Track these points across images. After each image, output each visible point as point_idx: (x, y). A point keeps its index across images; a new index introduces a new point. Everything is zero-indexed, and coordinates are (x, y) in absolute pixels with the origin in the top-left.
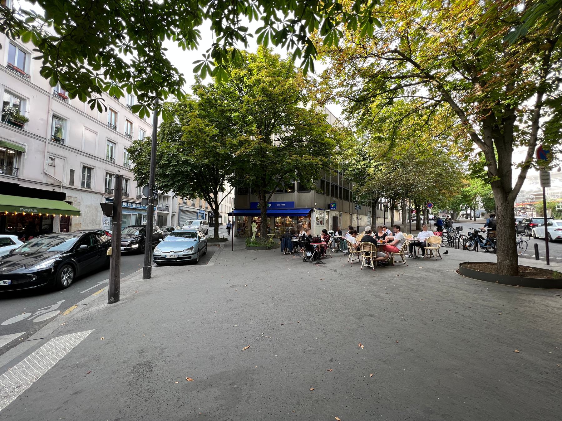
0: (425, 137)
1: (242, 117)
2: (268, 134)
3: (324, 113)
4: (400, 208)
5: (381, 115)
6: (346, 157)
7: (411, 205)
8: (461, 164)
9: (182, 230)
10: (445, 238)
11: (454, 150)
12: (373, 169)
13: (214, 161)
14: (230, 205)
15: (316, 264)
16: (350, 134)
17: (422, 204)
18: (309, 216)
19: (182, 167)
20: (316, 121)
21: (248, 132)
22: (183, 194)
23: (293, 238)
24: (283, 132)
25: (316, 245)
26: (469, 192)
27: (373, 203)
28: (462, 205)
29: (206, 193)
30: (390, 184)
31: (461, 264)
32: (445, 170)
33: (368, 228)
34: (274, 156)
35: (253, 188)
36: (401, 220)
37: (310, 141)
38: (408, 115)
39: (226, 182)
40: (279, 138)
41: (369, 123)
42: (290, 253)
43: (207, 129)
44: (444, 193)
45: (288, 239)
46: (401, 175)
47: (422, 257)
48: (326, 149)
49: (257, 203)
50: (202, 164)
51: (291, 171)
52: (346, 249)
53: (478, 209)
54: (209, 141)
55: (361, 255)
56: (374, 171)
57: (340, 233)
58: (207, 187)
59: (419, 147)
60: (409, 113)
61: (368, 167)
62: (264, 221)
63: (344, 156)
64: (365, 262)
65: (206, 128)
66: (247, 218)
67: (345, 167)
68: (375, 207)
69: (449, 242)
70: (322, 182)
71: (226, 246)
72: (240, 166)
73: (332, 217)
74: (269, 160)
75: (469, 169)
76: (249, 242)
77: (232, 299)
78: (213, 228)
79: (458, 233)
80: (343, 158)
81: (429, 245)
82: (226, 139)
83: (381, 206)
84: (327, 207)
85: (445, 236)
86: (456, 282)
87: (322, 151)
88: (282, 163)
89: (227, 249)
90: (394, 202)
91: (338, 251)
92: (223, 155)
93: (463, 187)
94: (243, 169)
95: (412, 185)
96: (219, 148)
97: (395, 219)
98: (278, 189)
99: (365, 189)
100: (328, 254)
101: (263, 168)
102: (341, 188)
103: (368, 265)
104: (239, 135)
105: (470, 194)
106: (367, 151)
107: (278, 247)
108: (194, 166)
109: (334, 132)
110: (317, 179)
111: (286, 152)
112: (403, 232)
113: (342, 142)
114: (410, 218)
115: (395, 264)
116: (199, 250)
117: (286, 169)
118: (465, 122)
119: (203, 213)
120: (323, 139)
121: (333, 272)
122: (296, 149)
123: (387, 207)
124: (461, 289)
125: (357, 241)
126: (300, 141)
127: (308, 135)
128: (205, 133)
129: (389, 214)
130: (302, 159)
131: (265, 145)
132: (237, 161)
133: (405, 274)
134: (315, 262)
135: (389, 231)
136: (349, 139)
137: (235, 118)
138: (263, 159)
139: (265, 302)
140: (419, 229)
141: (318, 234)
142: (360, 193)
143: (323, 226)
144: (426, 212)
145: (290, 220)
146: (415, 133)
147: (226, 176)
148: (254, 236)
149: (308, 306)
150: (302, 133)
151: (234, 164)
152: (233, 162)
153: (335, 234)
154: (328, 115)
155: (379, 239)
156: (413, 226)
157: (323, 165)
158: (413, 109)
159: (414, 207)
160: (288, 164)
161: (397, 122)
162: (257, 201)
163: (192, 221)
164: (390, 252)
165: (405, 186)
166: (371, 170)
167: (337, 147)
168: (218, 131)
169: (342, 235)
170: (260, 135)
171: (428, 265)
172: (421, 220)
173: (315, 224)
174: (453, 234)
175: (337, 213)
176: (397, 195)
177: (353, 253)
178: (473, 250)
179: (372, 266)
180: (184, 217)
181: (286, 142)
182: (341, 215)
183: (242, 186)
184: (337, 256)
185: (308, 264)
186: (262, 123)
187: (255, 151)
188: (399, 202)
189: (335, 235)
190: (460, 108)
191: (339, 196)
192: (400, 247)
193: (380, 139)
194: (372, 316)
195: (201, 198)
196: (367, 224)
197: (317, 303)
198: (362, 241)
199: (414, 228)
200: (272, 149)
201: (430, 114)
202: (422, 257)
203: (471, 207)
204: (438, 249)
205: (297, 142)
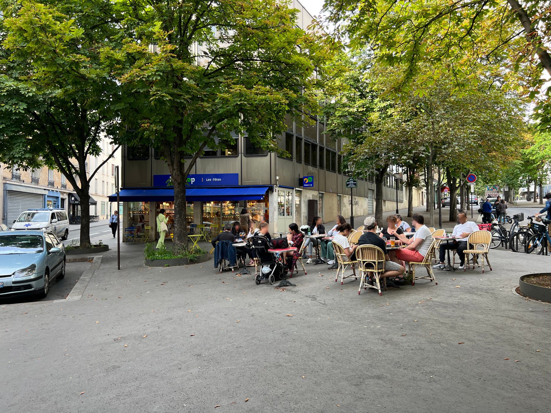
0: (465, 58)
1: (131, 5)
2: (185, 44)
3: (291, 7)
4: (423, 183)
5: (391, 14)
6: (331, 93)
7: (442, 178)
8: (522, 107)
9: (12, 232)
10: (497, 235)
11: (513, 81)
12: (377, 114)
13: (77, 92)
14: (112, 180)
15: (280, 286)
16: (336, 47)
17: (459, 177)
18: (266, 199)
19: (6, 103)
20: (277, 21)
21: (144, 37)
22: (10, 159)
23: (237, 240)
24: (214, 40)
25: (279, 252)
26: (533, 155)
27: (377, 175)
28: (521, 178)
29: (62, 157)
30: (407, 141)
31: (523, 278)
32: (497, 117)
33: (370, 220)
34: (198, 85)
35: (158, 148)
36: (425, 204)
37: (265, 60)
38: (438, 17)
39: (102, 135)
40: (207, 51)
41: (373, 29)
42: (230, 270)
43: (58, 26)
44: (494, 156)
45: (227, 244)
46: (425, 126)
47: (460, 267)
48: (296, 75)
49: (167, 177)
50: (51, 98)
51: (231, 115)
52: (332, 257)
53: (545, 184)
54: (64, 50)
55: (357, 268)
56: (380, 117)
57: (321, 230)
58: (63, 145)
59: (455, 75)
60: (441, 13)
61: (369, 111)
62: (181, 210)
63: (327, 90)
64: (365, 281)
65: (55, 24)
66: (147, 206)
67: (329, 111)
68: (381, 181)
69: (502, 241)
70: (289, 137)
71: (104, 261)
72: (130, 104)
73: (306, 200)
74: (188, 93)
75: (537, 116)
76: (151, 252)
77: (117, 364)
78: (79, 227)
79: (517, 224)
80: (325, 94)
81: (472, 247)
82: (99, 48)
83: (391, 181)
84: (297, 182)
85: (496, 231)
86: (516, 309)
87: (287, 79)
88: (214, 101)
89: (107, 266)
90: (414, 173)
91: (317, 262)
92: (95, 81)
93: (523, 146)
94: (137, 111)
95: (443, 143)
96: (85, 67)
97: (415, 203)
98: (206, 149)
99: (363, 150)
100: (300, 269)
101: (177, 108)
102: (321, 149)
103: (371, 286)
104: (127, 43)
105: (534, 158)
106: (367, 81)
107: (210, 259)
108: (32, 102)
109: (309, 42)
110: (279, 132)
111: (221, 79)
112: (428, 225)
113: (325, 63)
114: (440, 200)
115: (416, 281)
116: (47, 271)
117: (221, 111)
118: (532, 34)
119: (57, 198)
120: (289, 57)
121: (309, 301)
122: (240, 75)
123: (402, 182)
124: (524, 321)
125: (350, 243)
126: (247, 59)
127: (262, 48)
128: (54, 34)
129: (404, 194)
130: (250, 93)
131: (178, 64)
132: (124, 93)
133: (434, 299)
134: (278, 284)
135: (405, 225)
136: (336, 57)
137: (118, 7)
138: (175, 91)
139: (183, 366)
140: (454, 219)
141: (282, 231)
142: (356, 157)
143: (290, 217)
144: (465, 190)
145: (231, 207)
146: (450, 51)
147: (103, 123)
148: (161, 240)
149: (266, 367)
150: (250, 44)
151: (118, 99)
152: (115, 95)
153: (312, 231)
154: (298, 11)
155: (388, 239)
156: (445, 214)
157: (289, 105)
158: (447, 7)
159: (445, 181)
160: (225, 101)
161: (419, 28)
162: (166, 171)
163: (34, 214)
164: (407, 262)
165: (432, 144)
166: (374, 116)
167: (315, 73)
168: (82, 31)
169: (324, 233)
170: (170, 43)
171: (470, 280)
172: (458, 203)
173: (276, 213)
174: (508, 227)
175: (316, 193)
176: (418, 161)
177: (345, 265)
178: (539, 254)
179: (378, 286)
180: (14, 204)
181: (220, 60)
182: (322, 198)
183: (135, 142)
184: (316, 271)
185: (265, 287)
186: (172, 19)
187: (159, 75)
188: (421, 173)
189: (312, 234)
190: (523, 9)
191: (318, 163)
192: (424, 252)
193: (391, 59)
194: (379, 377)
195: (51, 166)
196: (367, 212)
197: (281, 361)
198: (360, 243)
199: (446, 217)
200: (193, 72)
201: (475, 18)
202: (460, 267)
203: (535, 180)
204: (486, 253)
205: (242, 60)
